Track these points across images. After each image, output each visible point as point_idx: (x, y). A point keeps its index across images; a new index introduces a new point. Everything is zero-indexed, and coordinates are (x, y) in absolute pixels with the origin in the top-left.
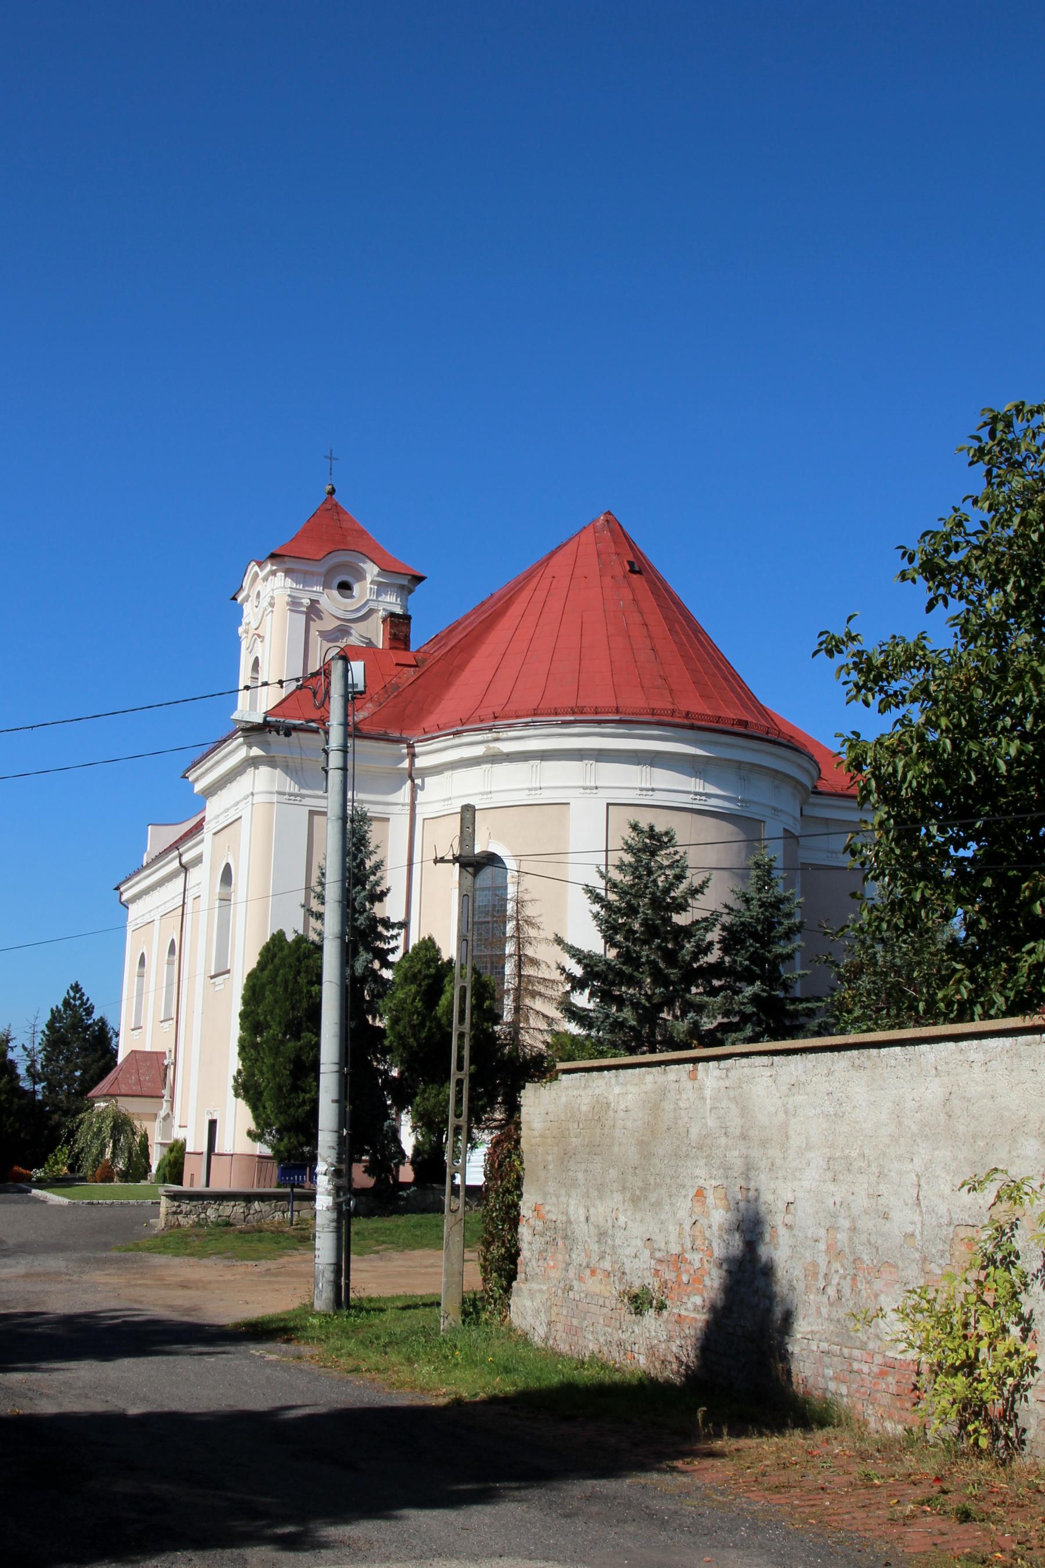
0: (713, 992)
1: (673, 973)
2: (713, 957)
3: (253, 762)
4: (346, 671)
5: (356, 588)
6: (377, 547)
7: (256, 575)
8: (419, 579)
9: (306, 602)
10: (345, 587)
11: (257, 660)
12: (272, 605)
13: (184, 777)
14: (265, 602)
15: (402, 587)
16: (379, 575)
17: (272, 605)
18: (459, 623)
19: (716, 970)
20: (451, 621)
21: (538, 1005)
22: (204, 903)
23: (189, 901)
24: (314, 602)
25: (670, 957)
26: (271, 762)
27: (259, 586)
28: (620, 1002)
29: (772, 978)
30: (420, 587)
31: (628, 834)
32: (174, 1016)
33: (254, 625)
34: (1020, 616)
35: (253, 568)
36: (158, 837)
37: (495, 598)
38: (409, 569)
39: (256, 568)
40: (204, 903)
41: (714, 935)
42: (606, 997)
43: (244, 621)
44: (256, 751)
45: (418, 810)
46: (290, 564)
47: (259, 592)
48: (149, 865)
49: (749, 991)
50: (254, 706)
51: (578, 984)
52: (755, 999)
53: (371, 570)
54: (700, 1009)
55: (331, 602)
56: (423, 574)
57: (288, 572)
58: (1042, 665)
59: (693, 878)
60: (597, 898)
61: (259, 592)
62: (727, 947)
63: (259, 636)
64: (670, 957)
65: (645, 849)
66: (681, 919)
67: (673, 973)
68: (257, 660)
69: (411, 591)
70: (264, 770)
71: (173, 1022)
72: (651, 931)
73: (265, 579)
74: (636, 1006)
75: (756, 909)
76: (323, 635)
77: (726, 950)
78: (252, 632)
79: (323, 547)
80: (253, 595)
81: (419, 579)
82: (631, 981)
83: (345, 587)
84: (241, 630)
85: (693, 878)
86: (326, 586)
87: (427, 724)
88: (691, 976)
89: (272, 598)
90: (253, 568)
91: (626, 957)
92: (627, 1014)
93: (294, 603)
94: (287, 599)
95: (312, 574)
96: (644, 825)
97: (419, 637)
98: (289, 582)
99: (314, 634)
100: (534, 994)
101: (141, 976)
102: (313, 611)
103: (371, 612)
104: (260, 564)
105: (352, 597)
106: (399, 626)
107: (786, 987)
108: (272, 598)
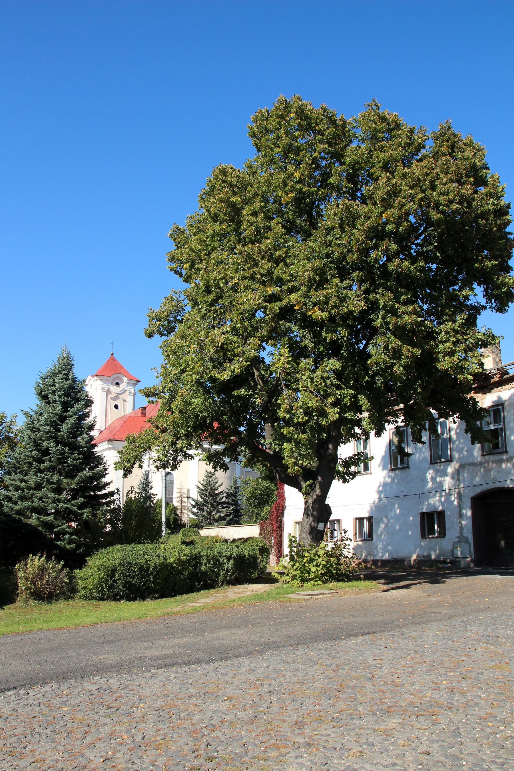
0: (224, 508)
1: (215, 504)
2: (223, 500)
3: (109, 449)
6: (126, 371)
9: (107, 389)
19: (224, 503)
21: (186, 512)
24: (109, 389)
25: (214, 500)
26: (114, 449)
28: (203, 510)
29: (237, 505)
31: (205, 473)
34: (156, 571)
41: (224, 495)
42: (200, 509)
44: (110, 446)
46: (102, 377)
49: (232, 508)
51: (194, 507)
52: (233, 510)
53: (125, 379)
54: (221, 512)
55: (114, 389)
57: (101, 380)
59: (219, 483)
60: (198, 488)
62: (227, 497)
64: (214, 500)
65: (209, 476)
66: (216, 492)
67: (215, 504)
70: (112, 451)
72: (210, 495)
74: (207, 512)
75: (233, 489)
77: (227, 498)
82: (206, 506)
85: (219, 483)
86: (112, 384)
88: (219, 504)
91: (205, 501)
92: (205, 513)
93: (103, 389)
96: (209, 471)
98: (102, 383)
99: (109, 398)
100: (185, 509)
102: (108, 391)
103: (125, 391)
104: (92, 376)
107: (240, 506)
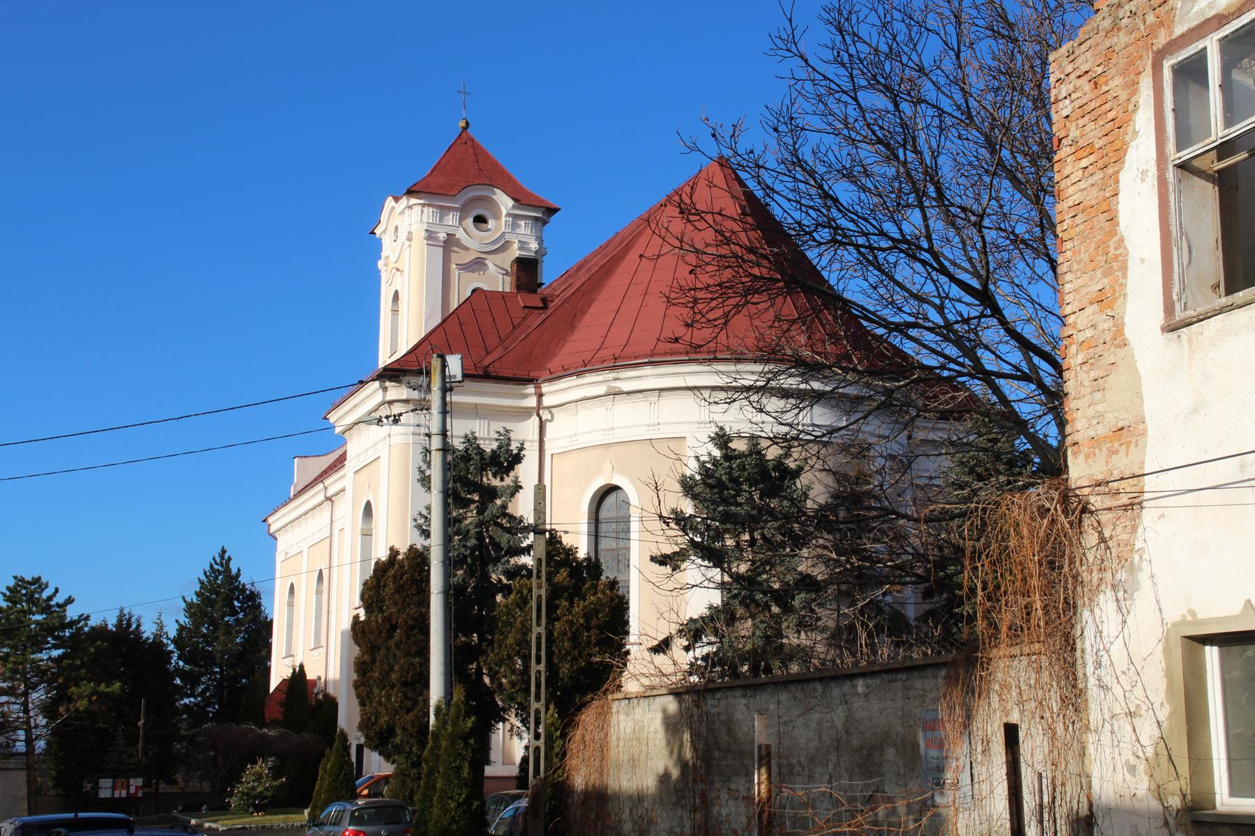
4: (444, 366)
5: (491, 223)
7: (393, 208)
8: (552, 211)
9: (442, 236)
10: (480, 220)
11: (396, 293)
12: (409, 239)
13: (325, 418)
14: (403, 236)
15: (536, 219)
16: (514, 207)
17: (409, 239)
18: (586, 261)
20: (580, 258)
22: (348, 532)
23: (336, 533)
27: (396, 221)
30: (554, 219)
32: (323, 643)
33: (392, 259)
35: (390, 202)
36: (303, 469)
37: (618, 239)
38: (541, 201)
39: (393, 203)
40: (348, 532)
43: (384, 254)
45: (547, 446)
47: (397, 228)
48: (297, 495)
50: (385, 358)
53: (505, 202)
56: (557, 205)
58: (381, 814)
61: (397, 228)
63: (398, 270)
68: (396, 293)
69: (545, 223)
71: (323, 650)
73: (402, 213)
76: (463, 267)
78: (392, 265)
79: (460, 177)
80: (391, 230)
81: (552, 211)
83: (480, 220)
84: (380, 263)
87: (554, 364)
89: (410, 233)
90: (390, 202)
93: (430, 236)
94: (423, 234)
95: (450, 209)
97: (549, 274)
101: (291, 605)
102: (450, 243)
104: (397, 199)
105: (488, 230)
106: (527, 269)
108: (410, 233)
